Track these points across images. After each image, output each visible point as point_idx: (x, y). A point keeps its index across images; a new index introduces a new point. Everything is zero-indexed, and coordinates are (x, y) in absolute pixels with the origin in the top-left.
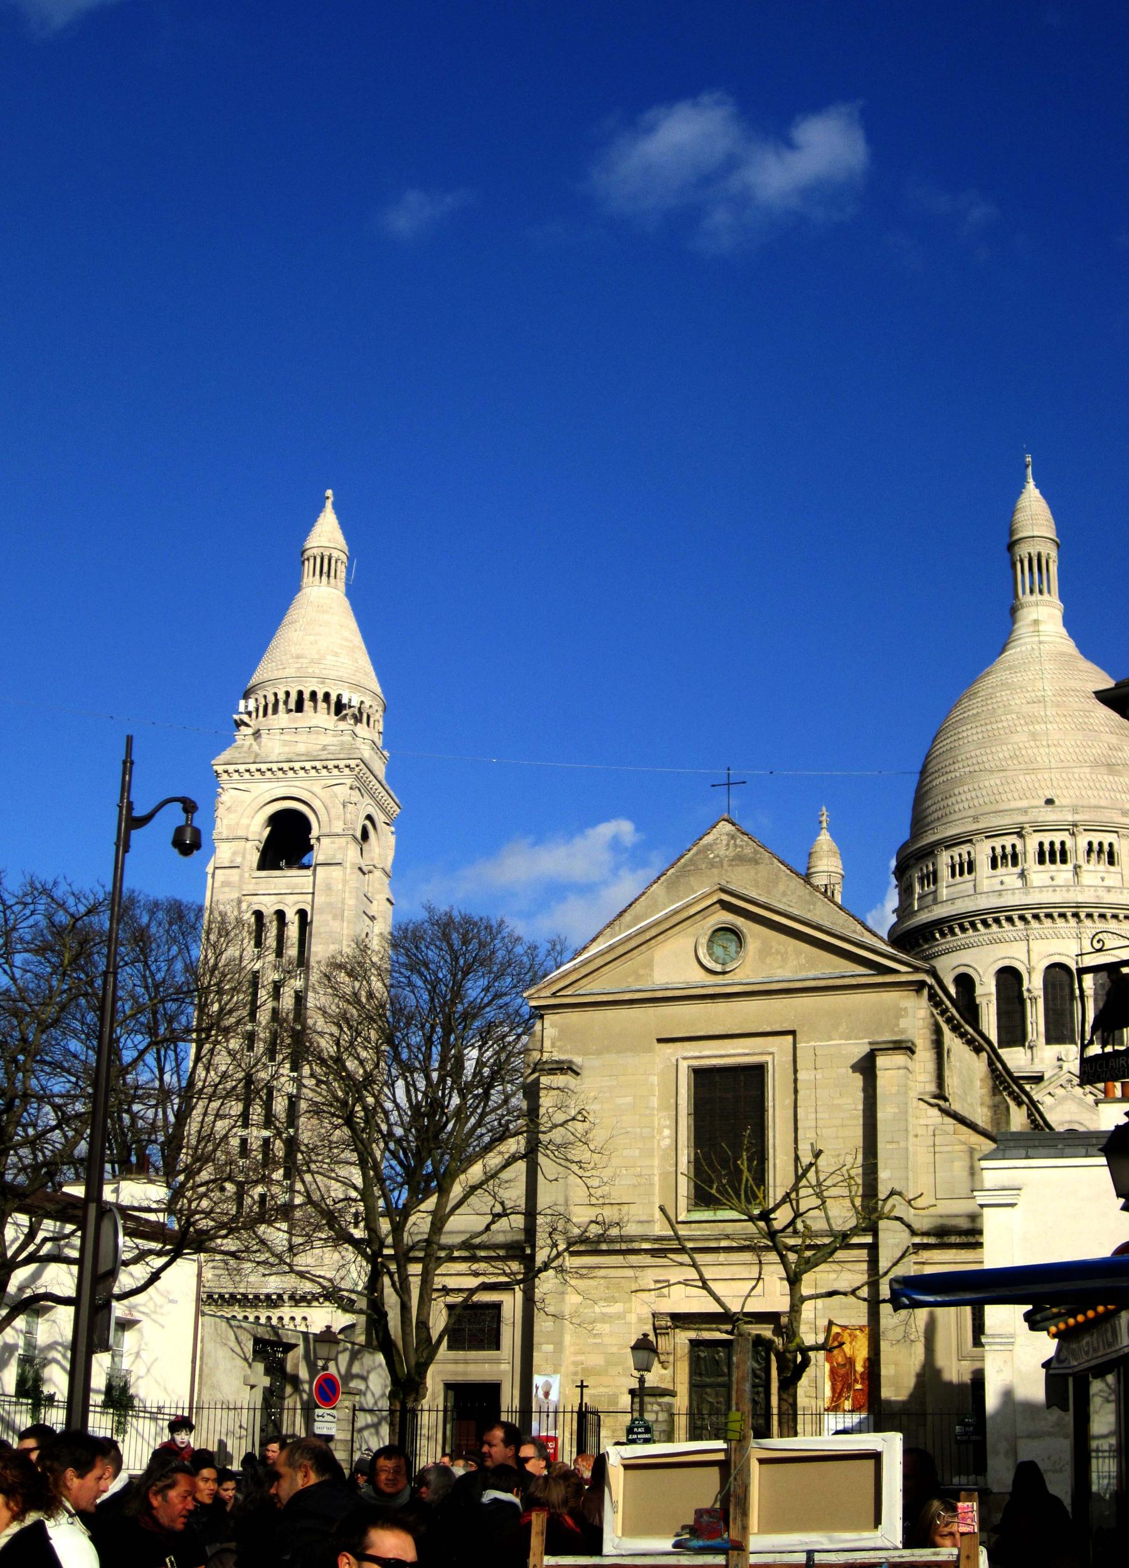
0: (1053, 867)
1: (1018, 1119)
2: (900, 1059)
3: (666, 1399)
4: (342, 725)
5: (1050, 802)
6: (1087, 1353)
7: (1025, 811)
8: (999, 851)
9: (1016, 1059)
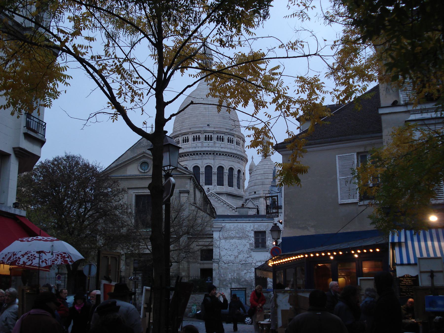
0: (220, 142)
2: (186, 195)
5: (208, 125)
7: (202, 127)
8: (195, 137)
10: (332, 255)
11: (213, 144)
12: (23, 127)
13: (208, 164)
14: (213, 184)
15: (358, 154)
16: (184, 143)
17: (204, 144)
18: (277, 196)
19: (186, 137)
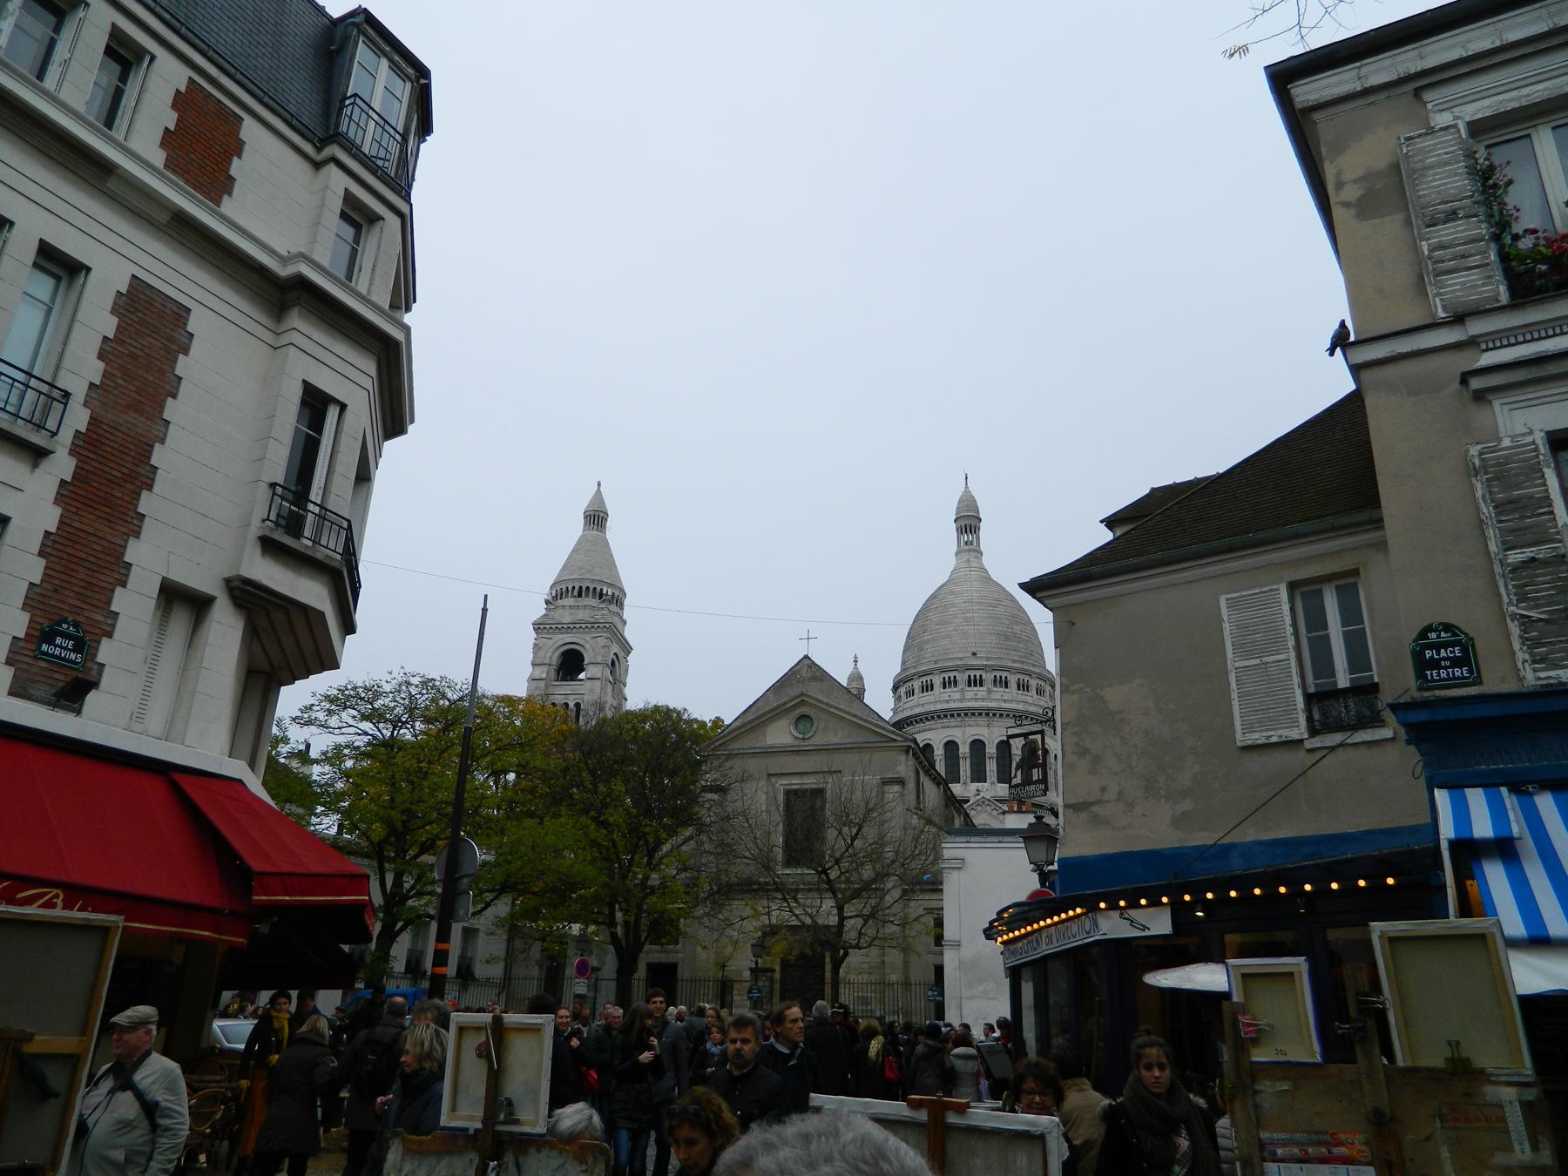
0: (1001, 690)
1: (958, 823)
2: (896, 788)
3: (769, 974)
4: (602, 606)
5: (974, 654)
6: (1021, 954)
7: (961, 659)
8: (947, 679)
9: (956, 789)
10: (1200, 901)
11: (985, 693)
12: (260, 521)
13: (977, 737)
14: (988, 778)
15: (1293, 587)
16: (923, 692)
17: (966, 693)
18: (1042, 732)
19: (927, 681)
